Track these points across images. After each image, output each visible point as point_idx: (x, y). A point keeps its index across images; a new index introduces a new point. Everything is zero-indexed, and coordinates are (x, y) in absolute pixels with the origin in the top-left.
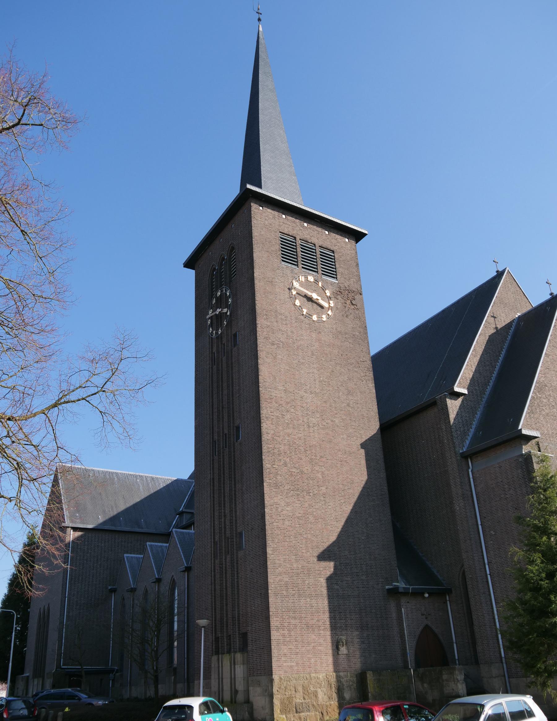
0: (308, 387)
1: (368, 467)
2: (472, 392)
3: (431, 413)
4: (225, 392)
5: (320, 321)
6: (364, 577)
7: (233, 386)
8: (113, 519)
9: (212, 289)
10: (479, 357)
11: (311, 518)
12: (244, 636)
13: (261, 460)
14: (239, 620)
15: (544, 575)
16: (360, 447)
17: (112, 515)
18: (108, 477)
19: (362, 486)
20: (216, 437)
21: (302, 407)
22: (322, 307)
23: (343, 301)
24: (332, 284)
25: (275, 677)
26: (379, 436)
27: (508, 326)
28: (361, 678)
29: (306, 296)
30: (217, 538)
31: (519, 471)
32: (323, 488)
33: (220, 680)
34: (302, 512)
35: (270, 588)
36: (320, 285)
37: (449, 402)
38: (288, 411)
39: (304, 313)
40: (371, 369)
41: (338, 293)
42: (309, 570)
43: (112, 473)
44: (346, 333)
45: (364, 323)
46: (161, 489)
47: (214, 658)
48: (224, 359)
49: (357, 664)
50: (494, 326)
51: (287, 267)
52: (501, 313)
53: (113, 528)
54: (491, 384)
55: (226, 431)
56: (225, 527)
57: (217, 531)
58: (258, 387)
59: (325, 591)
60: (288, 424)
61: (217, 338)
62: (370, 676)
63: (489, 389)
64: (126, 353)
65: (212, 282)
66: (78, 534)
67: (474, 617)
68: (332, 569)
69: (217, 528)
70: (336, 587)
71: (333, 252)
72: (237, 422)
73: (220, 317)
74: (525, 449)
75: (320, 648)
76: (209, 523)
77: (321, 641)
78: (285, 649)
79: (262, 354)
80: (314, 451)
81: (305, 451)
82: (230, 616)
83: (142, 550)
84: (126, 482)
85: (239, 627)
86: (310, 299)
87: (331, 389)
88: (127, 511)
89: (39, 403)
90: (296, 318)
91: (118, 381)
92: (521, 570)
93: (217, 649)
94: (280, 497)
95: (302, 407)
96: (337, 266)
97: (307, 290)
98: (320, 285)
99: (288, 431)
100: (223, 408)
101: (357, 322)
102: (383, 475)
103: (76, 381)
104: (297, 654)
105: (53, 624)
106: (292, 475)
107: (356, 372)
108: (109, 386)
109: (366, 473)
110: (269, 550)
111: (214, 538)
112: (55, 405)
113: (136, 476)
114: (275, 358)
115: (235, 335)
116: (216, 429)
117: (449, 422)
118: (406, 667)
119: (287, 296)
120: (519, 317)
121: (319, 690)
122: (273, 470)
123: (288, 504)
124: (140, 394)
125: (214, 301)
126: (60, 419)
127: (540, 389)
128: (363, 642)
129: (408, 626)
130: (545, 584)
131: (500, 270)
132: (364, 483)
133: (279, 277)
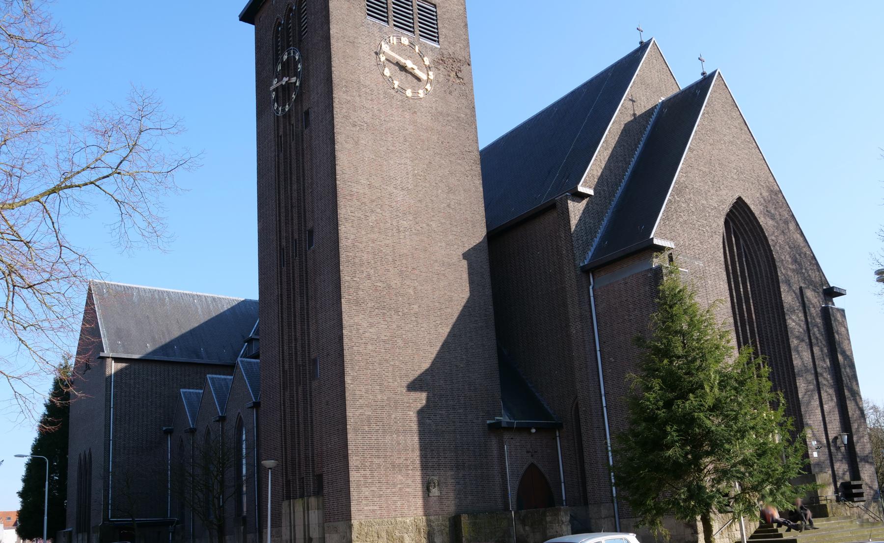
0: (399, 182)
1: (471, 282)
2: (600, 194)
3: (550, 218)
4: (295, 187)
5: (416, 98)
6: (461, 411)
7: (304, 180)
8: (165, 348)
9: (277, 51)
10: (611, 150)
11: (400, 342)
12: (319, 478)
13: (339, 271)
14: (313, 461)
15: (661, 403)
16: (461, 257)
17: (163, 343)
18: (157, 297)
19: (463, 304)
20: (284, 244)
21: (391, 206)
22: (419, 79)
23: (446, 73)
24: (432, 49)
25: (355, 522)
26: (486, 245)
27: (649, 113)
28: (455, 523)
29: (397, 64)
30: (287, 367)
31: (647, 288)
32: (416, 307)
33: (292, 527)
34: (388, 334)
35: (348, 423)
36: (417, 51)
37: (571, 204)
38: (372, 211)
39: (396, 86)
40: (479, 162)
41: (441, 61)
42: (396, 402)
43: (163, 292)
44: (448, 115)
45: (472, 102)
46: (224, 312)
47: (285, 504)
48: (293, 144)
49: (450, 507)
50: (632, 112)
51: (374, 24)
52: (641, 96)
53: (165, 358)
54: (623, 184)
55: (296, 236)
56: (296, 353)
57: (287, 358)
58: (335, 179)
59: (415, 426)
60: (372, 227)
61: (284, 116)
62: (465, 520)
63: (620, 190)
64: (146, 123)
65: (277, 42)
66: (121, 365)
67: (585, 454)
68: (424, 402)
69: (286, 353)
70: (428, 421)
71: (435, 6)
72: (310, 225)
73: (286, 89)
74: (656, 262)
75: (407, 490)
76: (277, 349)
77: (409, 482)
78: (366, 492)
79: (339, 138)
80: (404, 262)
81: (394, 260)
82: (302, 456)
83: (202, 384)
84: (181, 303)
85: (313, 468)
86: (403, 68)
87: (428, 185)
88: (183, 337)
89: (31, 187)
90: (385, 93)
91: (138, 162)
92: (636, 399)
93: (289, 491)
94: (361, 316)
95: (391, 206)
96: (440, 25)
97: (400, 55)
98: (417, 51)
99: (372, 236)
100: (292, 207)
101: (463, 101)
102: (488, 292)
103: (81, 160)
104: (380, 496)
105: (97, 471)
106: (376, 290)
107: (459, 164)
108: (125, 166)
109: (467, 289)
110: (348, 379)
111: (283, 366)
112: (53, 191)
113: (193, 296)
114: (357, 143)
115: (307, 113)
116: (284, 234)
117: (570, 229)
118: (506, 509)
119: (373, 62)
120: (663, 102)
121: (406, 536)
122: (353, 284)
123: (371, 325)
124: (169, 178)
125: (279, 68)
126: (64, 210)
127: (679, 191)
128: (458, 483)
129: (511, 464)
130: (662, 413)
131: (645, 41)
132: (465, 301)
133: (363, 37)
